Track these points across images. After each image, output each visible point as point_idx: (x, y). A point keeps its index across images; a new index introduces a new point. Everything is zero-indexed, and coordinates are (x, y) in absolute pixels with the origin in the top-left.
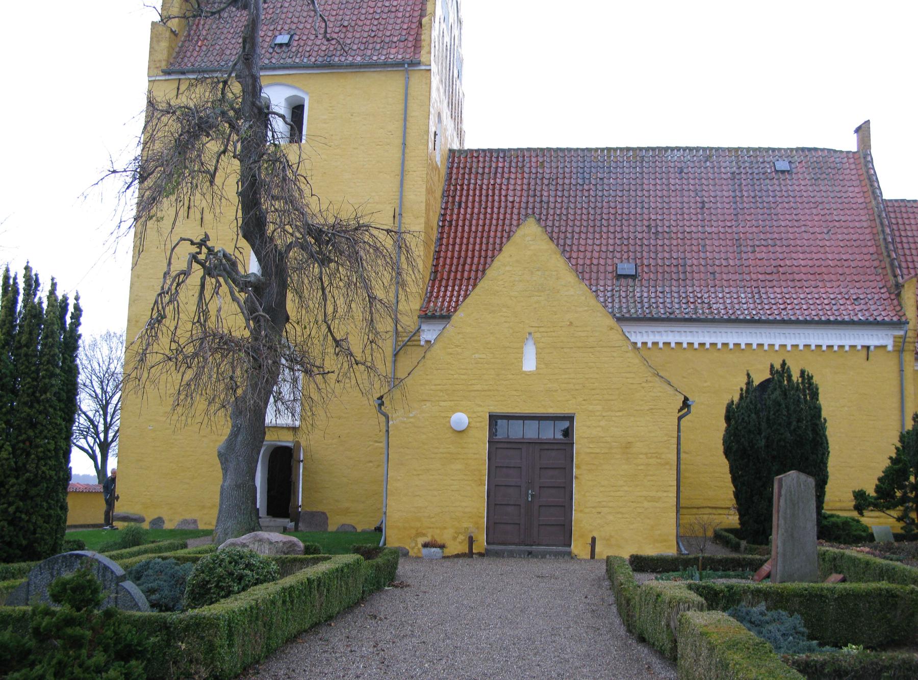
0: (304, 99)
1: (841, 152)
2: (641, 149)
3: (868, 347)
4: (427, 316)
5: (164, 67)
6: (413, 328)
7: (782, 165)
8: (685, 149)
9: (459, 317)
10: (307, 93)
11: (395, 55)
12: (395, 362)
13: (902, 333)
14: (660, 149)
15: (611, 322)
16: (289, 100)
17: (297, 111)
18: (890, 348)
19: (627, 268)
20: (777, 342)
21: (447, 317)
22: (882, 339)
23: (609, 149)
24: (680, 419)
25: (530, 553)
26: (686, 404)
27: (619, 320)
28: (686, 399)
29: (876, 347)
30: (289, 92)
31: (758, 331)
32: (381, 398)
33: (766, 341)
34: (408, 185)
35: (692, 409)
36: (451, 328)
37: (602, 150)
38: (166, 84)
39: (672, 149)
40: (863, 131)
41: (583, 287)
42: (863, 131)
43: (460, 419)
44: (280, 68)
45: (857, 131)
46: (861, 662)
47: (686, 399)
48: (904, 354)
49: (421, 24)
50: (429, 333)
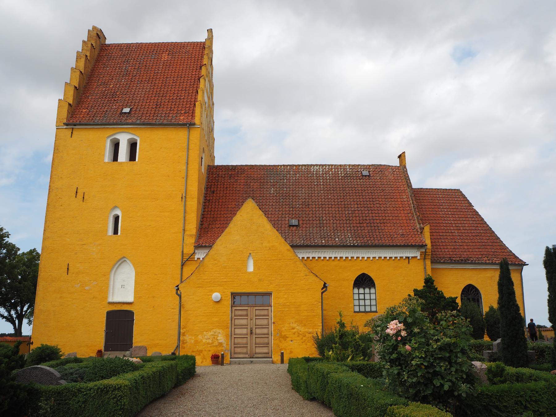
0: (137, 140)
1: (392, 166)
2: (299, 165)
3: (409, 257)
4: (198, 246)
5: (65, 121)
6: (192, 252)
7: (365, 173)
8: (320, 165)
9: (215, 247)
10: (138, 137)
11: (182, 119)
12: (182, 269)
13: (424, 250)
14: (308, 165)
15: (289, 247)
16: (129, 140)
17: (133, 146)
18: (419, 258)
19: (294, 222)
20: (371, 256)
21: (210, 247)
22: (416, 253)
23: (284, 166)
24: (322, 293)
25: (252, 362)
26: (325, 286)
27: (292, 246)
28: (325, 284)
29: (412, 257)
30: (130, 136)
31: (356, 251)
32: (177, 286)
33: (361, 256)
34: (189, 182)
35: (328, 289)
36: (213, 251)
37: (281, 166)
38: (66, 130)
39: (314, 165)
40: (401, 157)
41: (275, 230)
42: (401, 157)
43: (216, 296)
44: (124, 124)
45: (400, 157)
46: (291, 352)
47: (325, 284)
48: (426, 260)
49: (195, 105)
50: (200, 255)
